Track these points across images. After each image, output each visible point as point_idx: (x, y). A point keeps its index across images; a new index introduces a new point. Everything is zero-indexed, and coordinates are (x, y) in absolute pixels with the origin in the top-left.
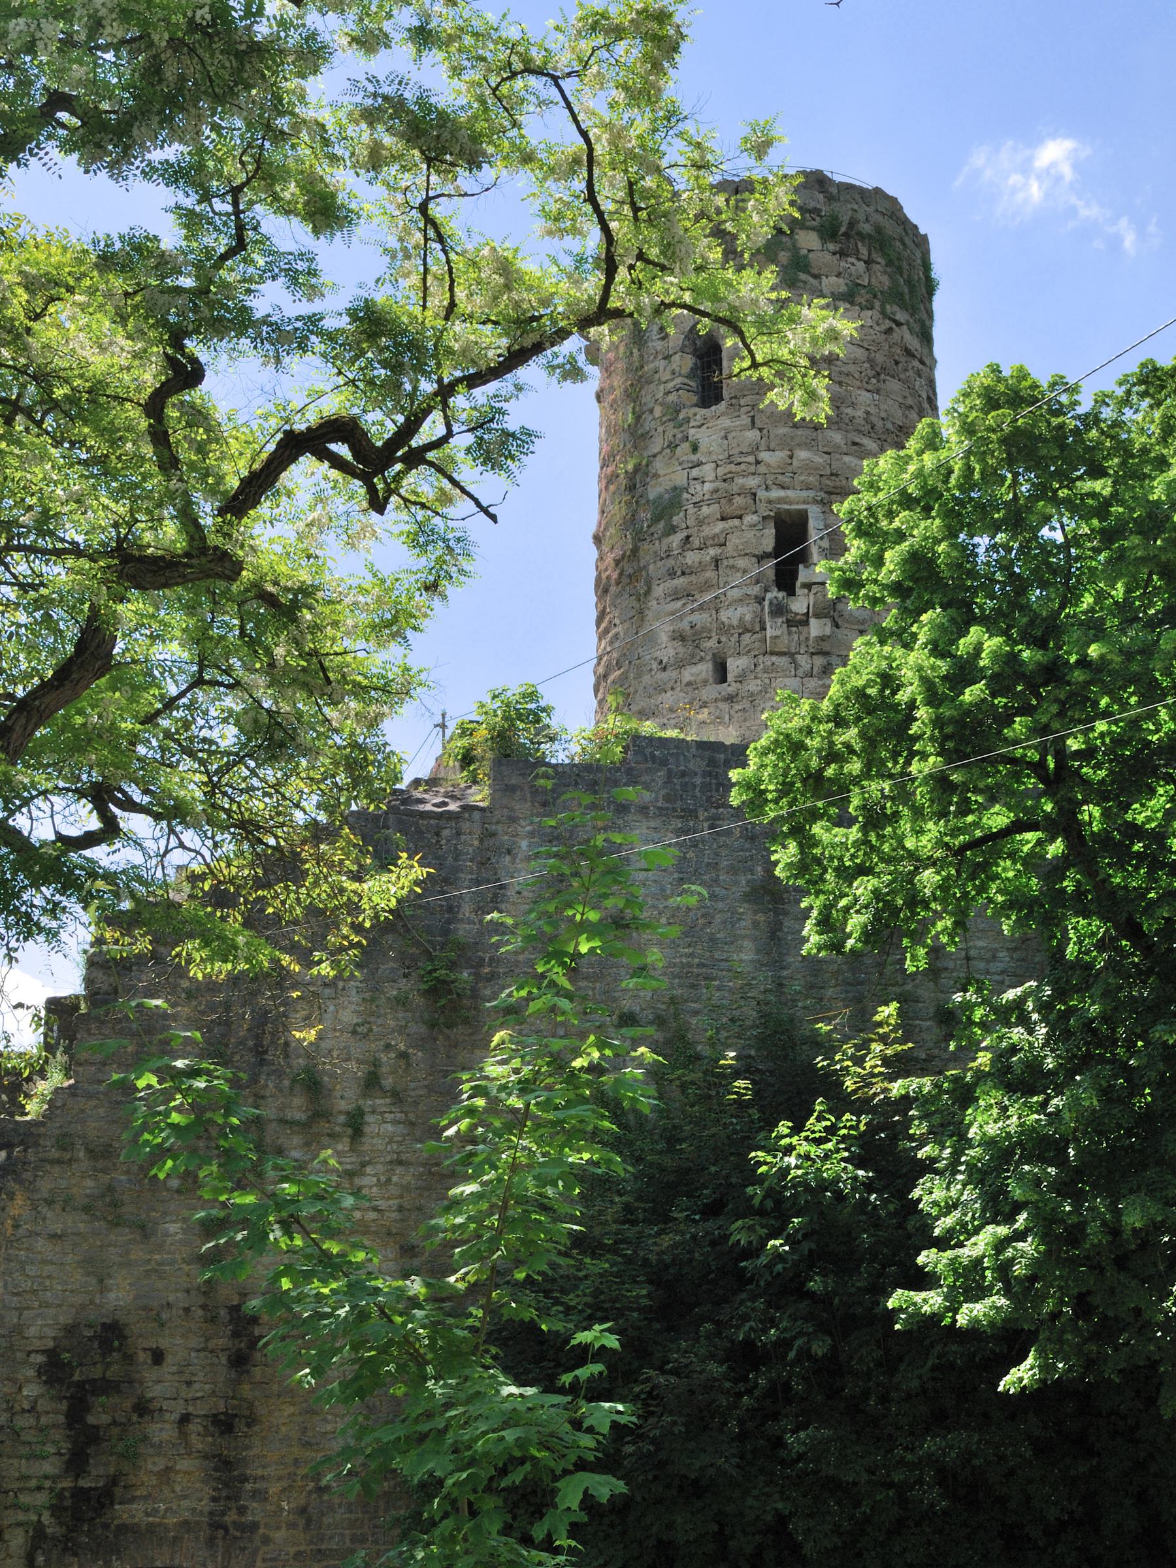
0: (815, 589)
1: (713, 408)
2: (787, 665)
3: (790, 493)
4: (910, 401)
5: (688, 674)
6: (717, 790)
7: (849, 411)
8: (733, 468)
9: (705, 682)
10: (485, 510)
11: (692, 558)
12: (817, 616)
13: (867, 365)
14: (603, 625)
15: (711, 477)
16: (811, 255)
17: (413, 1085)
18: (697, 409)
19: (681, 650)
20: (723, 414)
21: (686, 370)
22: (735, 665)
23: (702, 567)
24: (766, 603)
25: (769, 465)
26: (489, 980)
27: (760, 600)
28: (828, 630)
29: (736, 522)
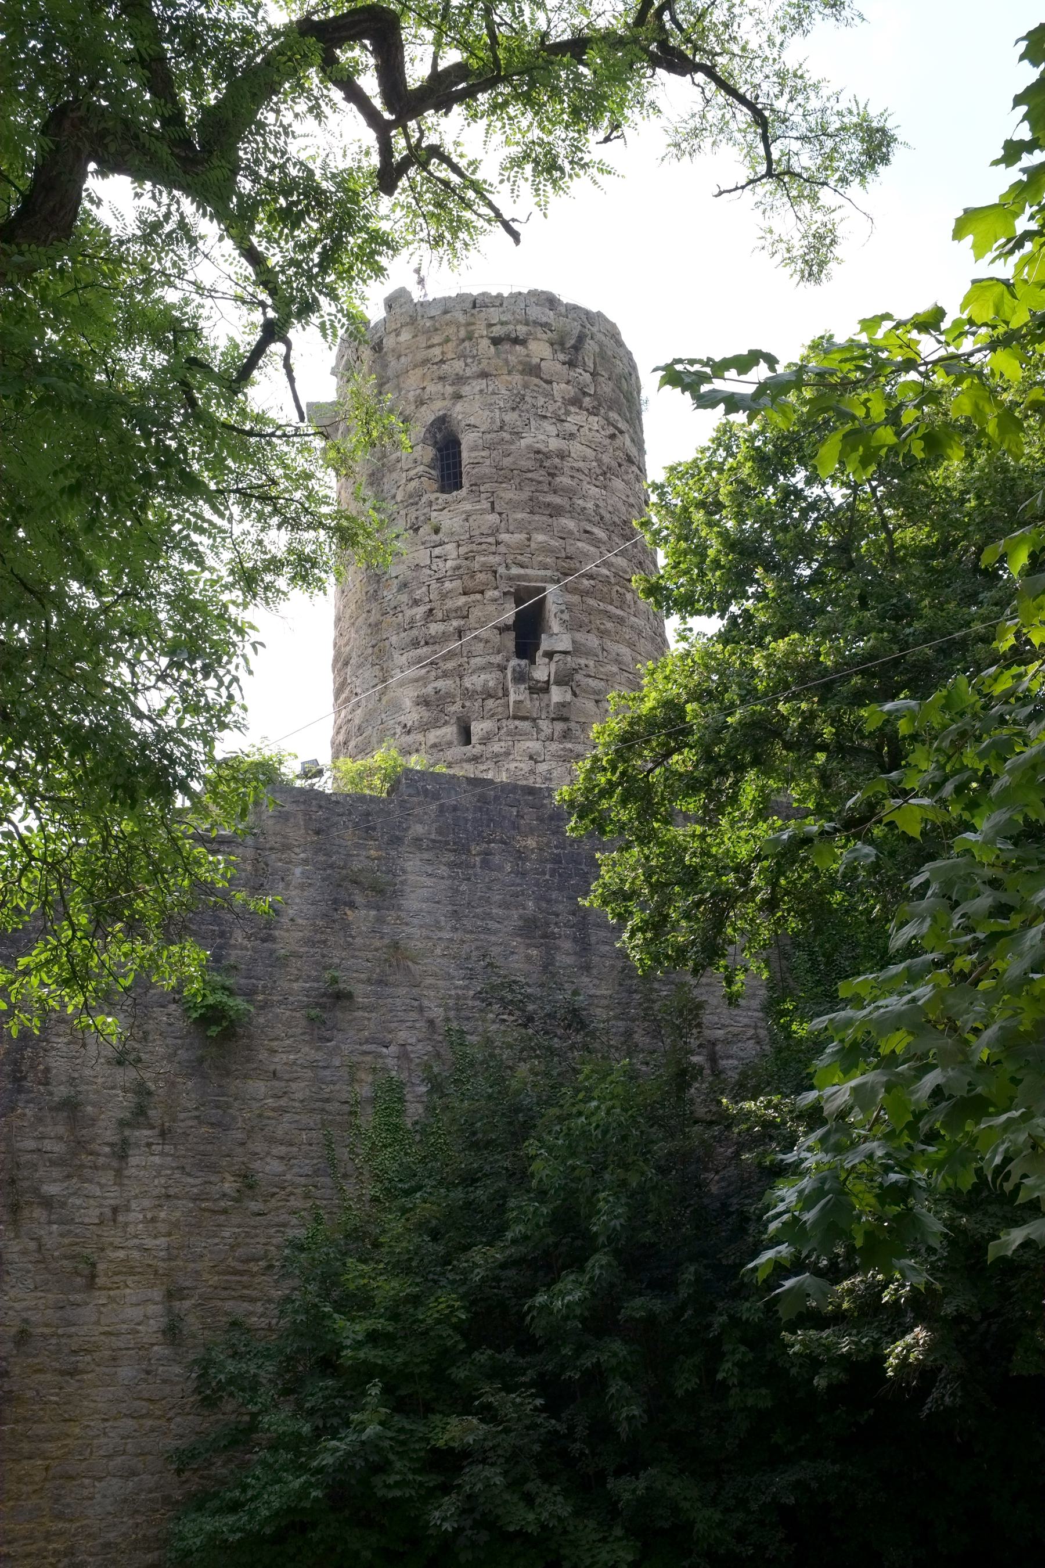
0: (556, 657)
1: (455, 493)
2: (529, 728)
3: (529, 571)
4: (632, 500)
5: (433, 736)
6: (488, 826)
7: (580, 502)
8: (474, 547)
9: (450, 744)
10: (507, 226)
11: (435, 628)
12: (558, 683)
13: (594, 464)
14: (344, 696)
15: (454, 555)
16: (543, 364)
17: (182, 1116)
18: (438, 495)
19: (426, 714)
20: (464, 499)
21: (427, 460)
22: (478, 728)
23: (445, 638)
24: (509, 672)
25: (508, 546)
26: (262, 1008)
27: (502, 668)
28: (569, 697)
29: (478, 596)
